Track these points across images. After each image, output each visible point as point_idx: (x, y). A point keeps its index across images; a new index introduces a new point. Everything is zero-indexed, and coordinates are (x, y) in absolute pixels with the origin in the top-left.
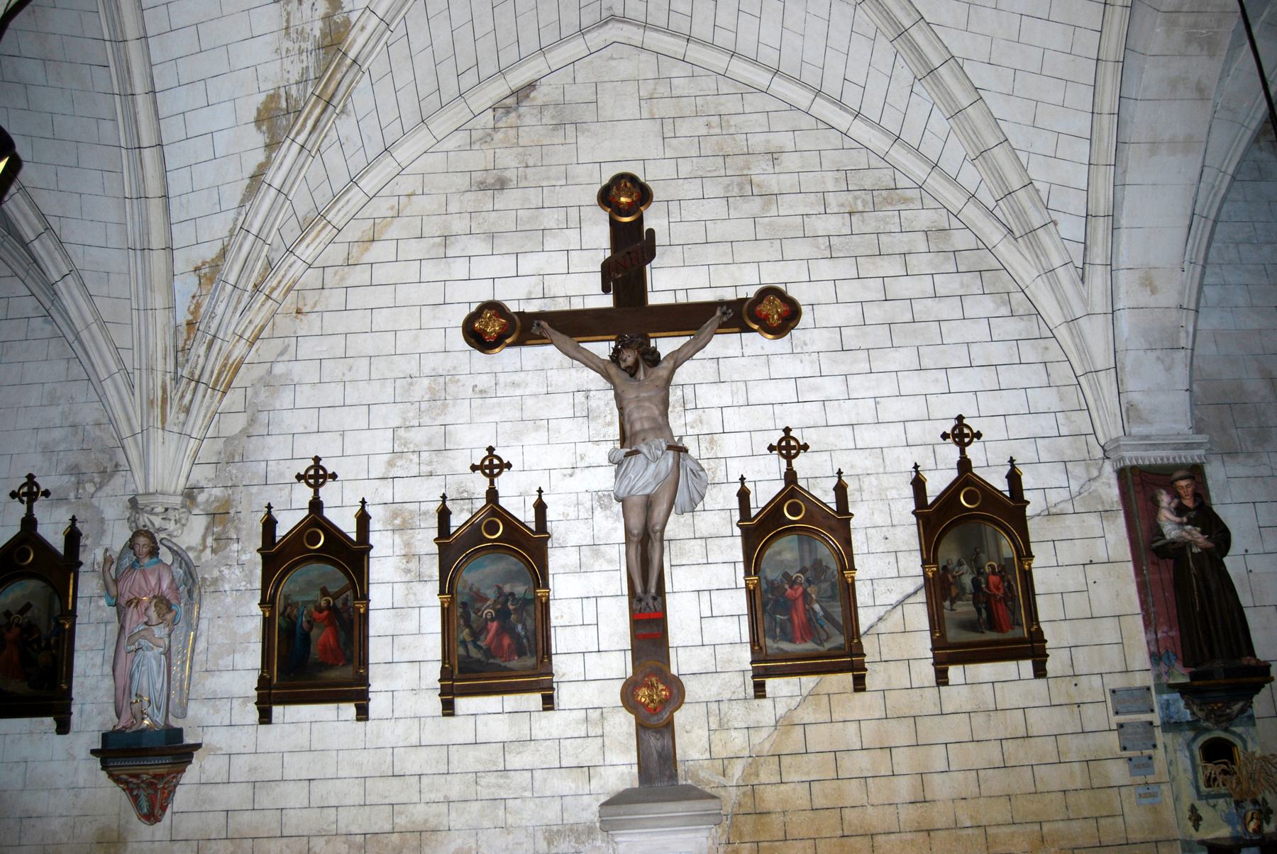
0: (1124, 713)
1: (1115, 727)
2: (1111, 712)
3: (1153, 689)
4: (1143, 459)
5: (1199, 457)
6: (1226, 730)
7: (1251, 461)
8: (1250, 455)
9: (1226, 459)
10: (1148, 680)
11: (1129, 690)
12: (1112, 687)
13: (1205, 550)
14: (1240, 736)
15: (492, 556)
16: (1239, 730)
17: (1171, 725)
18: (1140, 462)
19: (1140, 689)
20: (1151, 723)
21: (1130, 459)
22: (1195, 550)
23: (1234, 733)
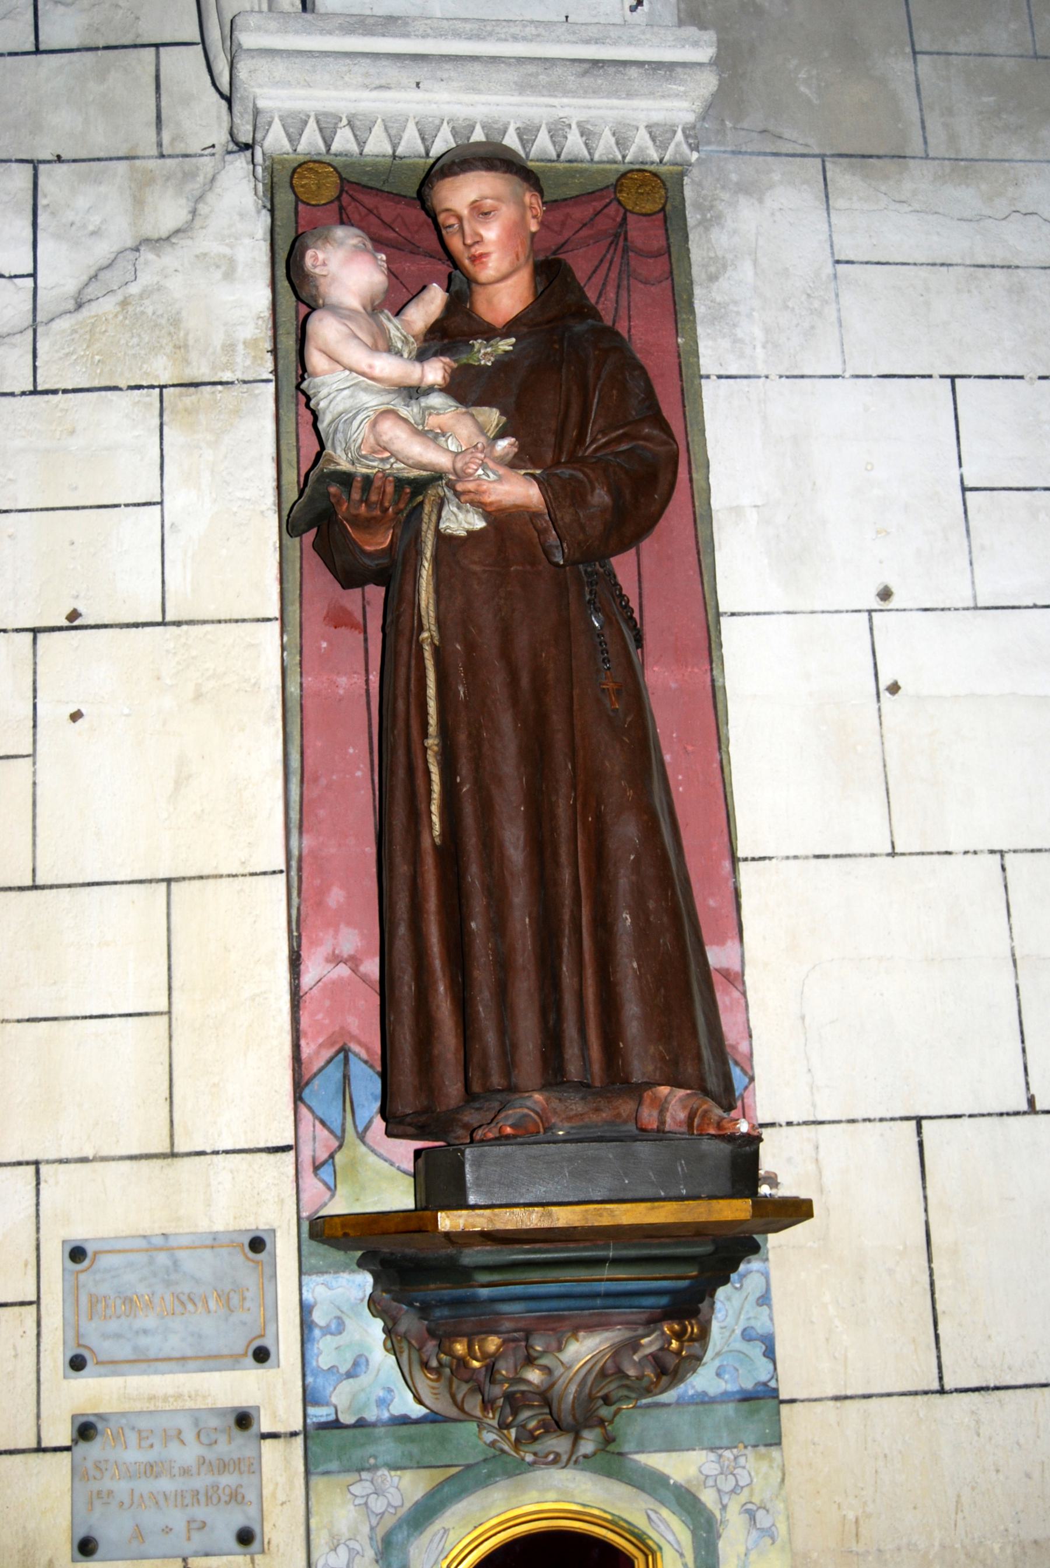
0: (113, 1366)
1: (60, 1434)
2: (55, 1358)
3: (285, 1249)
4: (359, 127)
5: (660, 134)
6: (610, 1461)
7: (966, 197)
8: (961, 167)
9: (840, 176)
10: (267, 1195)
11: (158, 1246)
12: (79, 1233)
13: (502, 521)
14: (685, 1501)
15: (368, 61)
16: (680, 1466)
17: (330, 1442)
18: (344, 142)
19: (214, 1242)
20: (244, 1420)
21: (557, 132)
22: (461, 521)
23: (653, 1484)
